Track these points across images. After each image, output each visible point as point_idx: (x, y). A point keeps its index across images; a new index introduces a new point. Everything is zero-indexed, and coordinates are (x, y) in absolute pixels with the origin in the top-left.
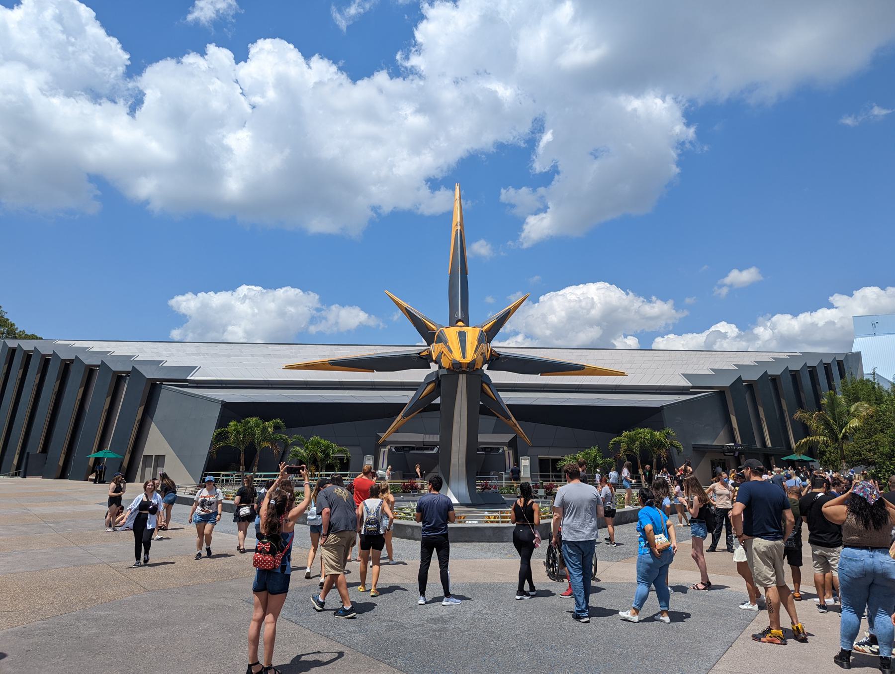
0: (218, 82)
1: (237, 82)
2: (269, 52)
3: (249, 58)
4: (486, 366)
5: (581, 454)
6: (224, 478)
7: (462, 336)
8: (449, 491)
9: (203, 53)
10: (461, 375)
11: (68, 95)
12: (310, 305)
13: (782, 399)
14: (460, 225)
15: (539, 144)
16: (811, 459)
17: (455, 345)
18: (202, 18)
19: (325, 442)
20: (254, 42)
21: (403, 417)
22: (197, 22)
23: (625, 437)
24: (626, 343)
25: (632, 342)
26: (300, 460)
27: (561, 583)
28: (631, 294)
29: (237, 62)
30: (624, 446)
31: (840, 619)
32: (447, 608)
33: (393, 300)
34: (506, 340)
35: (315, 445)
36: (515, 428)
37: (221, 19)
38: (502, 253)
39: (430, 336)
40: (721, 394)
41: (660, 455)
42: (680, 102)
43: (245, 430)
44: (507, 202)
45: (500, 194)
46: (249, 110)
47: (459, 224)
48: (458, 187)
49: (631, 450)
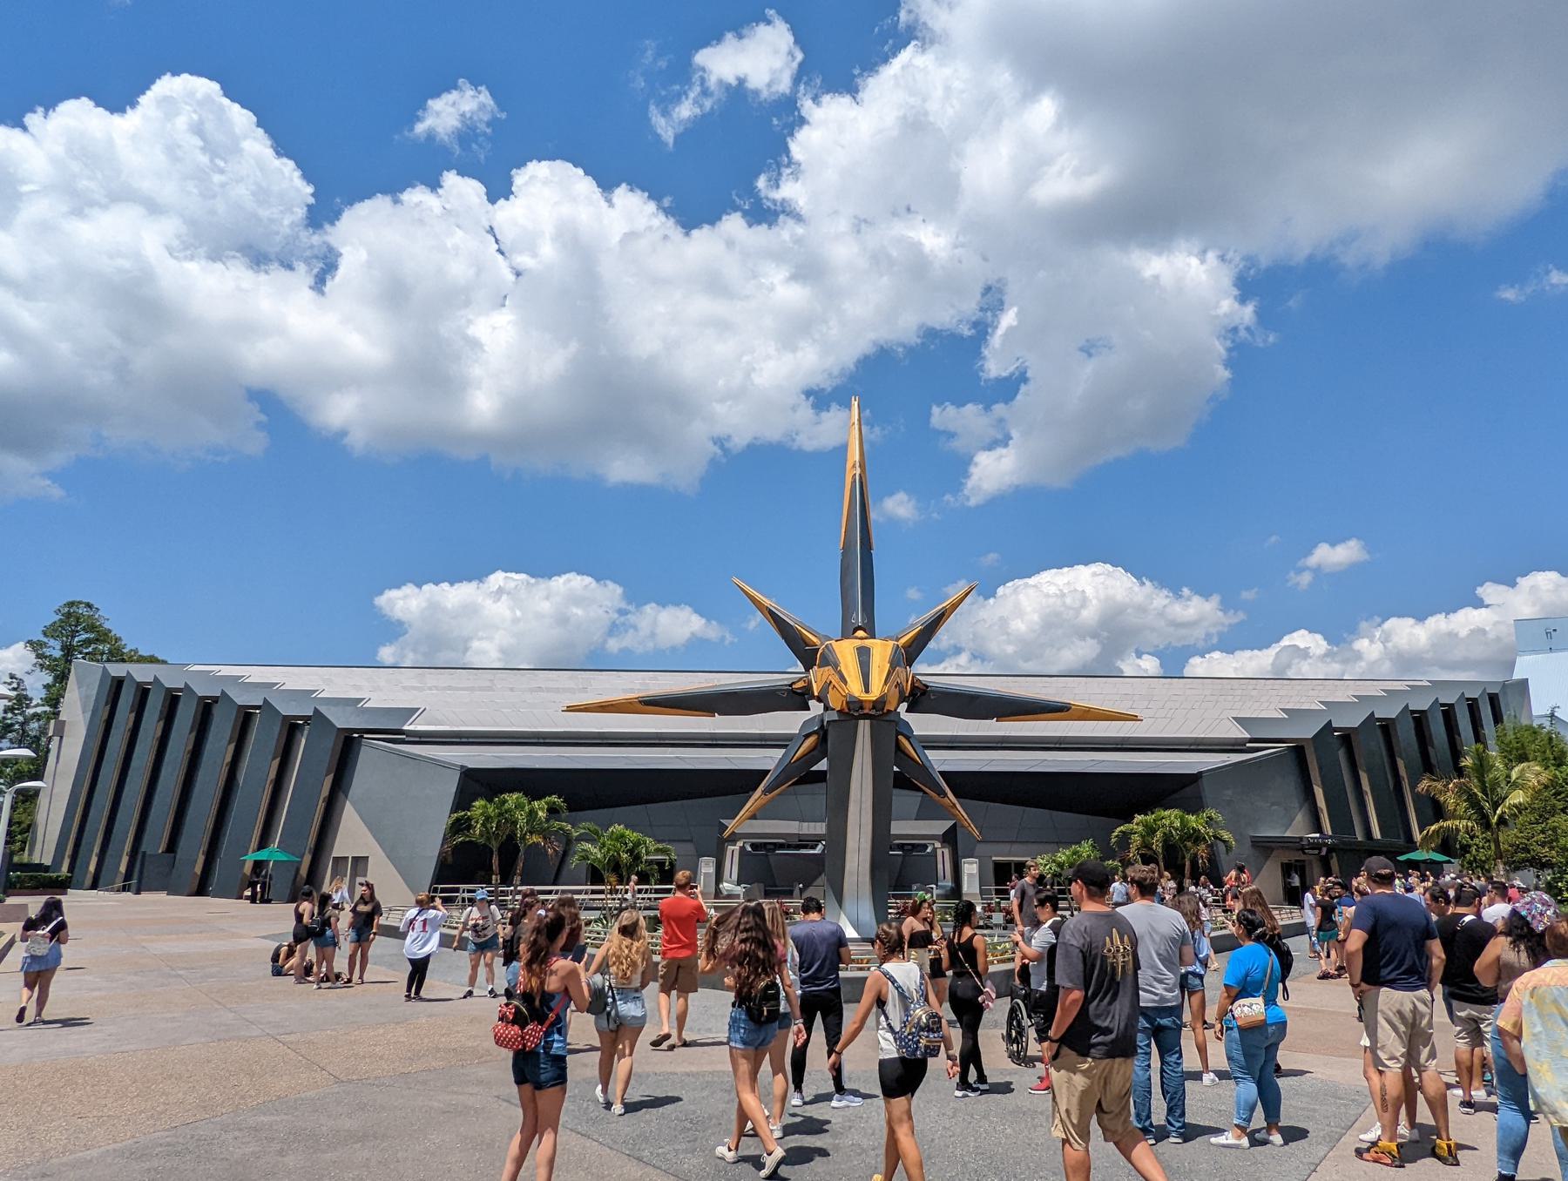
0: (460, 233)
1: (491, 230)
2: (546, 182)
3: (512, 193)
4: (904, 705)
5: (1064, 854)
6: (466, 895)
7: (864, 655)
8: (843, 915)
9: (434, 185)
10: (861, 722)
11: (215, 256)
12: (609, 604)
13: (1398, 760)
14: (860, 466)
15: (999, 322)
16: (1448, 858)
17: (852, 673)
18: (440, 130)
19: (633, 836)
20: (521, 164)
21: (765, 792)
22: (431, 136)
23: (1137, 824)
24: (1140, 666)
25: (1150, 664)
26: (592, 865)
27: (1031, 1070)
28: (1148, 583)
29: (492, 199)
30: (1136, 840)
31: (1495, 1124)
32: (841, 1113)
33: (742, 589)
34: (940, 661)
35: (617, 840)
36: (953, 810)
37: (469, 128)
38: (935, 515)
39: (808, 655)
40: (1298, 751)
41: (1196, 855)
42: (1230, 262)
43: (500, 814)
44: (942, 428)
45: (929, 415)
46: (512, 277)
47: (858, 464)
48: (856, 403)
49: (1147, 845)
